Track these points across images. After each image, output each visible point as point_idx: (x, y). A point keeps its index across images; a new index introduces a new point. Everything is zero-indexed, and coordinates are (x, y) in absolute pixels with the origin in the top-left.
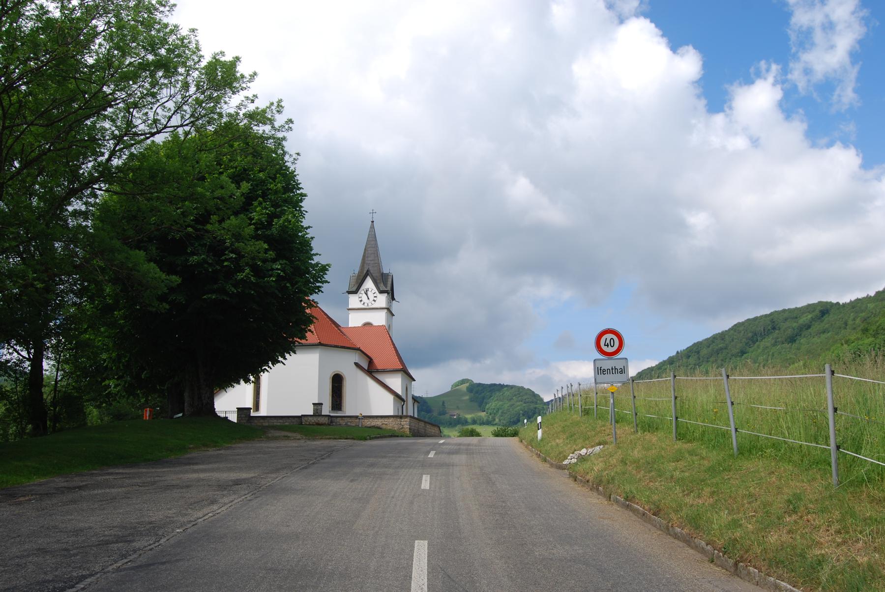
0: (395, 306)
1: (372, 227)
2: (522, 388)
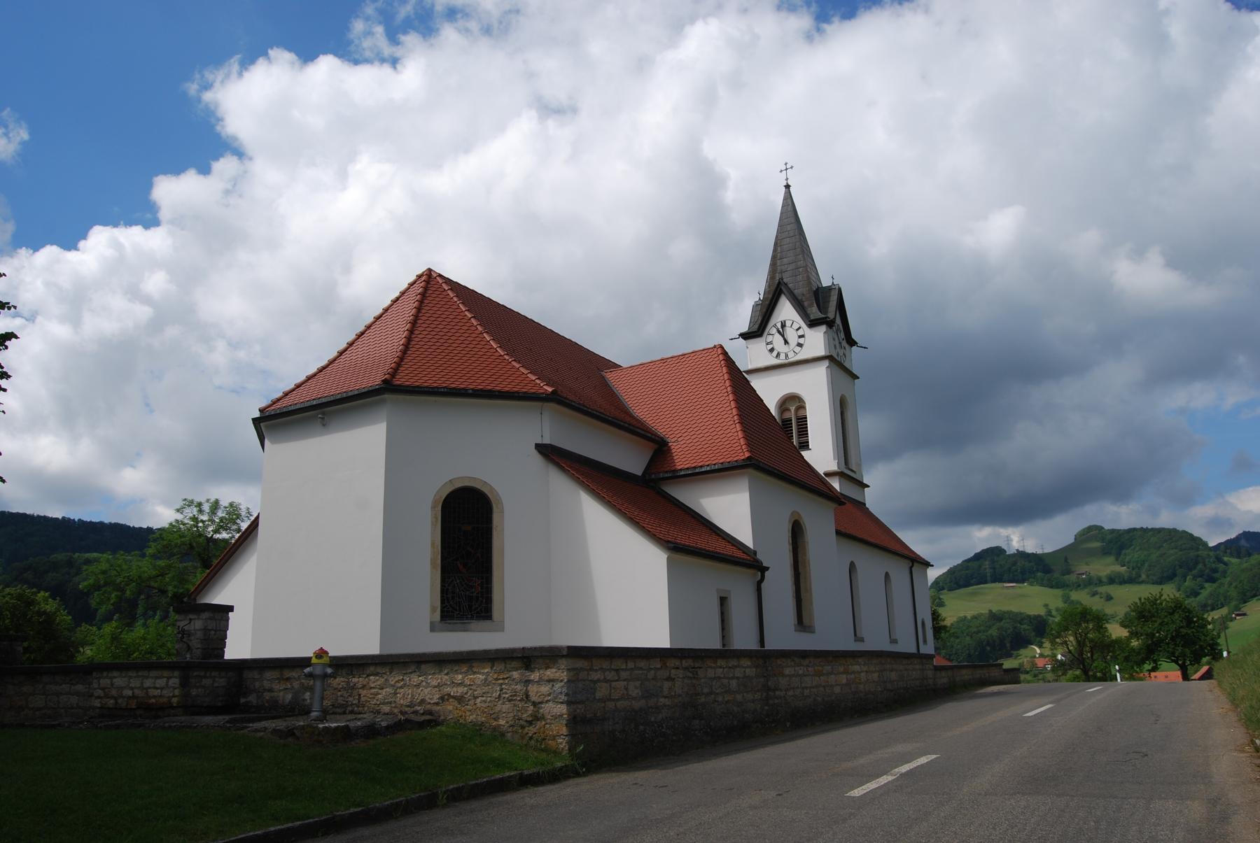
0: (856, 358)
1: (788, 198)
2: (1175, 530)
